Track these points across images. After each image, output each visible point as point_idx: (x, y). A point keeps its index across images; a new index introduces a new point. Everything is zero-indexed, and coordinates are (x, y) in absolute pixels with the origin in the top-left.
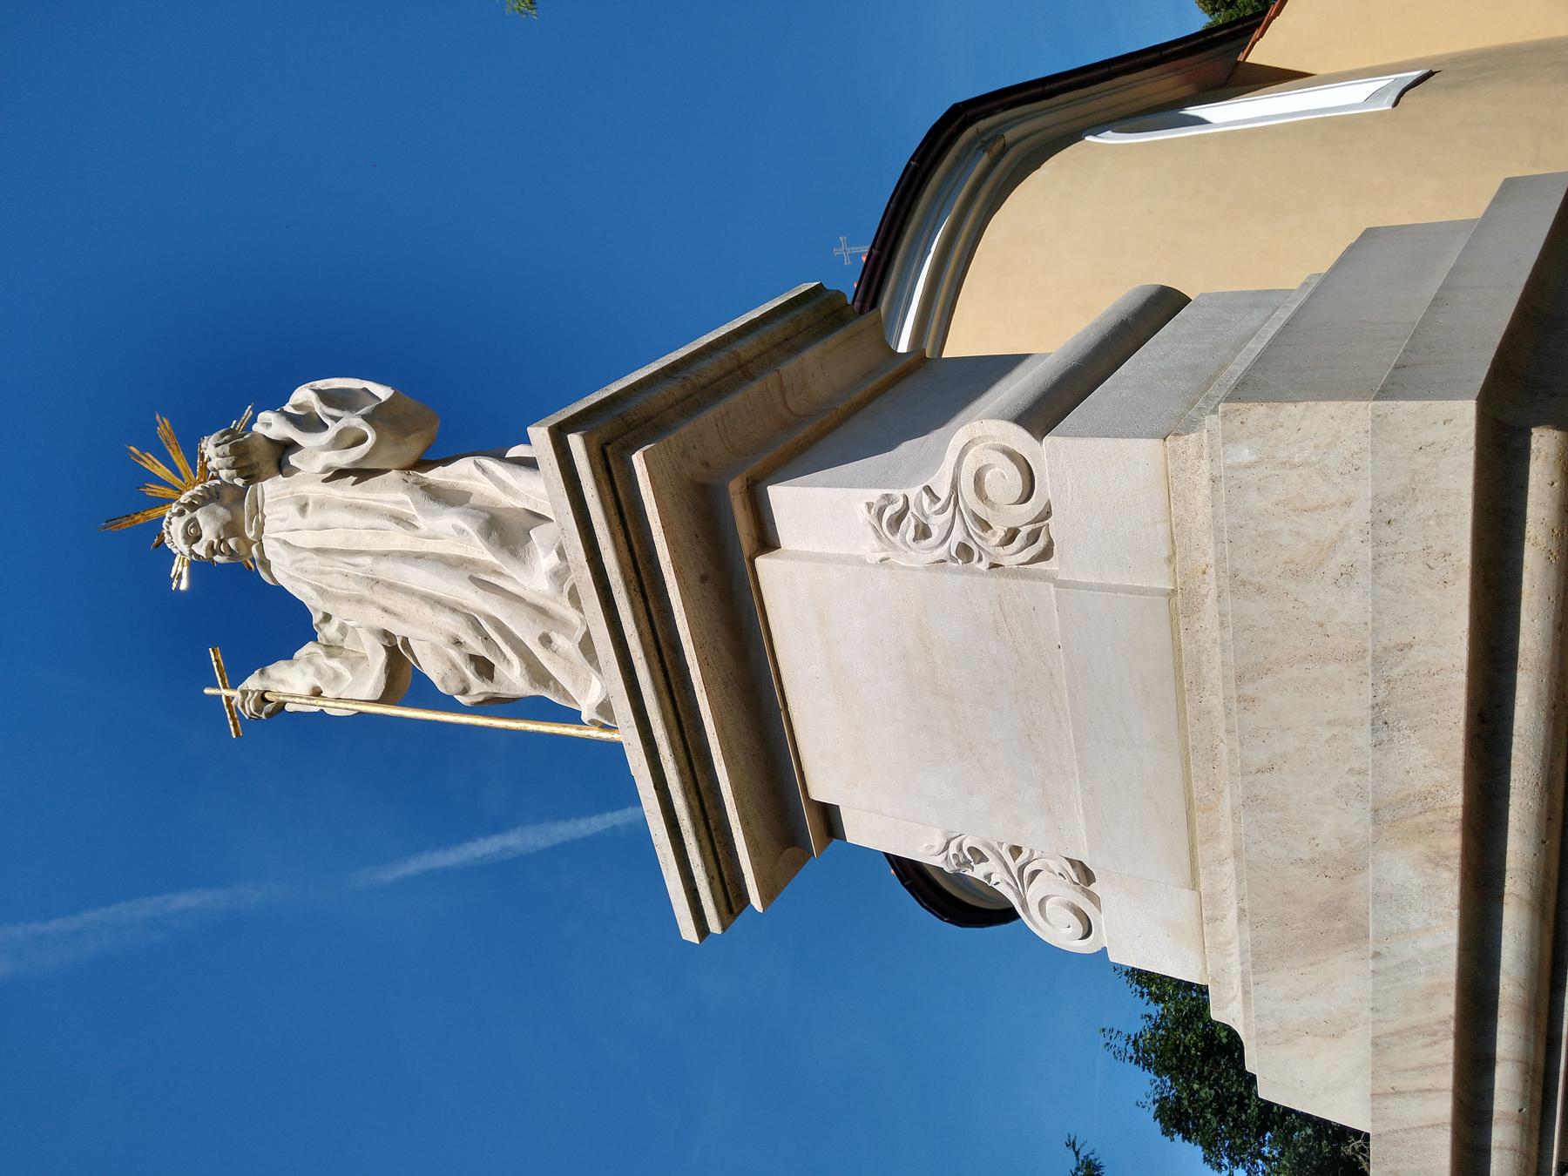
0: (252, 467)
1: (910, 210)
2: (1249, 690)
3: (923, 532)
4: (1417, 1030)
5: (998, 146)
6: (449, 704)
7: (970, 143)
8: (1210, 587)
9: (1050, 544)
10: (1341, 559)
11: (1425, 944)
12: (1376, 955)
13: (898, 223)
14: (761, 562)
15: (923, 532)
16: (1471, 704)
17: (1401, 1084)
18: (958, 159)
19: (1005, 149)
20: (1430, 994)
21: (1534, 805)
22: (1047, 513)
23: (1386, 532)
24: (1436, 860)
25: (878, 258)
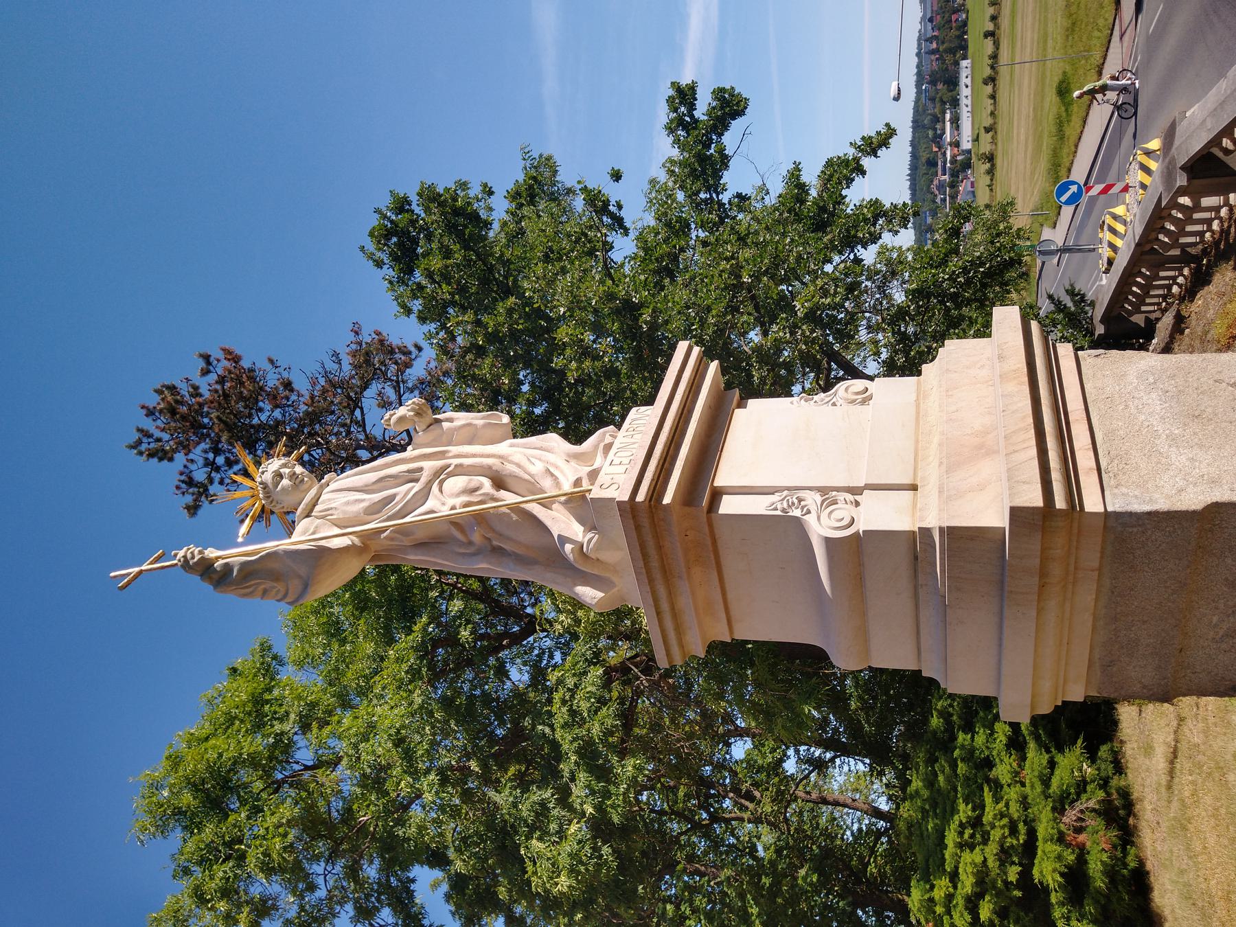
14: (738, 413)
17: (1016, 448)
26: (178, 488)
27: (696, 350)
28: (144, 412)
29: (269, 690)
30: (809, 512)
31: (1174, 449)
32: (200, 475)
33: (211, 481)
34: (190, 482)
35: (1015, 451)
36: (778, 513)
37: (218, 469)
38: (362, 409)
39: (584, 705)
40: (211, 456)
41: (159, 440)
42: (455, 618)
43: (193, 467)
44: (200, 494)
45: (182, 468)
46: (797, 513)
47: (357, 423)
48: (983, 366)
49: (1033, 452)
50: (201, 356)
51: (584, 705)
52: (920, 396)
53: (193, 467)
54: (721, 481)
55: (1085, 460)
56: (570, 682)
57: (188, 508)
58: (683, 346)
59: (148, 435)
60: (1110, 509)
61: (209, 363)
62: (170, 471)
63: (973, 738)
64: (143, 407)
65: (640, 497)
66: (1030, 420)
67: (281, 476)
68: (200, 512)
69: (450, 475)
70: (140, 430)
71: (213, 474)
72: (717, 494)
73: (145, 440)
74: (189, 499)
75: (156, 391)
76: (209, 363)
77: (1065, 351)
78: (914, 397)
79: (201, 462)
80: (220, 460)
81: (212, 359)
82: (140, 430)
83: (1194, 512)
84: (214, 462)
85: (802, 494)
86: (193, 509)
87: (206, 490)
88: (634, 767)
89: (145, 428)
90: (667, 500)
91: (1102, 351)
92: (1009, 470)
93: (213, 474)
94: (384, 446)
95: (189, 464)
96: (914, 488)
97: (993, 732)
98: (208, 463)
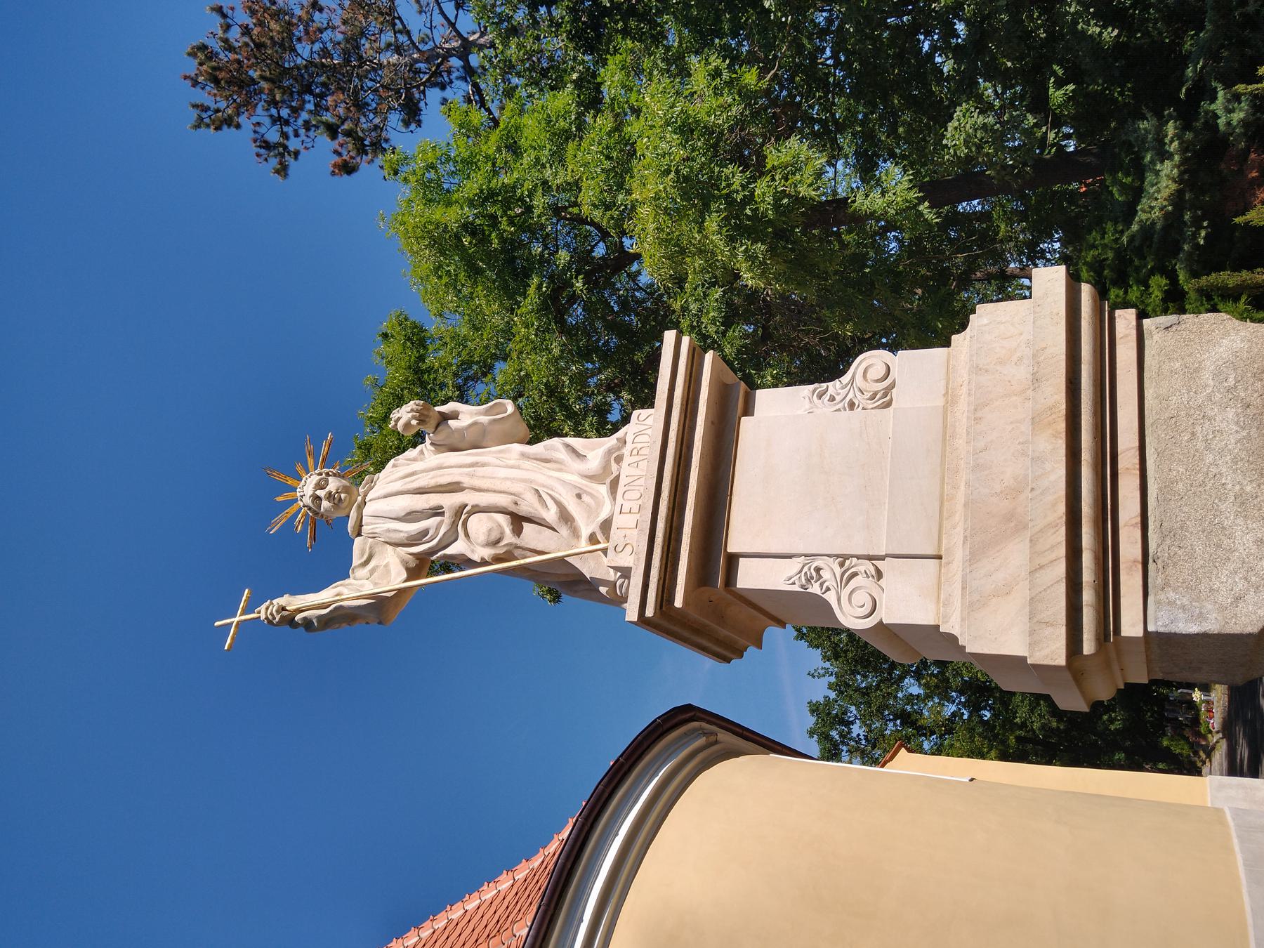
0: (427, 416)
1: (648, 748)
2: (979, 415)
3: (832, 399)
4: (1050, 526)
5: (712, 738)
6: (484, 563)
7: (695, 730)
8: (965, 389)
9: (891, 400)
10: (1018, 354)
11: (1052, 478)
12: (1032, 489)
13: (638, 752)
14: (745, 420)
15: (832, 399)
16: (1067, 387)
17: (1044, 561)
18: (686, 734)
19: (716, 742)
20: (1054, 505)
21: (1091, 487)
22: (893, 385)
23: (1038, 309)
24: (1055, 436)
25: (622, 764)
26: (258, 155)
27: (686, 340)
28: (189, 82)
29: (421, 358)
30: (828, 589)
31: (1240, 521)
32: (273, 136)
33: (285, 136)
34: (267, 146)
35: (1041, 567)
36: (797, 588)
37: (287, 123)
38: (399, 18)
39: (712, 329)
40: (274, 111)
41: (218, 111)
42: (564, 271)
43: (262, 130)
44: (282, 155)
45: (252, 135)
46: (815, 589)
47: (400, 32)
48: (1020, 359)
49: (1061, 569)
50: (213, 9)
51: (712, 329)
52: (949, 371)
53: (262, 130)
54: (732, 548)
55: (1129, 548)
56: (694, 307)
57: (277, 172)
58: (670, 336)
59: (205, 109)
60: (1151, 628)
61: (224, 16)
62: (240, 141)
63: (1126, 293)
64: (186, 78)
65: (649, 612)
66: (1062, 508)
67: (319, 498)
68: (290, 172)
69: (470, 514)
70: (195, 106)
71: (285, 129)
72: (733, 560)
73: (204, 115)
74: (274, 162)
75: (189, 54)
76: (224, 16)
77: (1125, 320)
78: (940, 402)
79: (267, 121)
80: (285, 113)
81: (225, 10)
82: (195, 106)
83: (1250, 635)
84: (280, 118)
85: (818, 563)
86: (283, 170)
87: (285, 147)
88: (772, 376)
89: (199, 102)
90: (678, 603)
91: (1173, 318)
92: (1032, 599)
93: (285, 129)
94: (438, 55)
95: (257, 129)
96: (940, 557)
97: (1148, 287)
98: (276, 120)
